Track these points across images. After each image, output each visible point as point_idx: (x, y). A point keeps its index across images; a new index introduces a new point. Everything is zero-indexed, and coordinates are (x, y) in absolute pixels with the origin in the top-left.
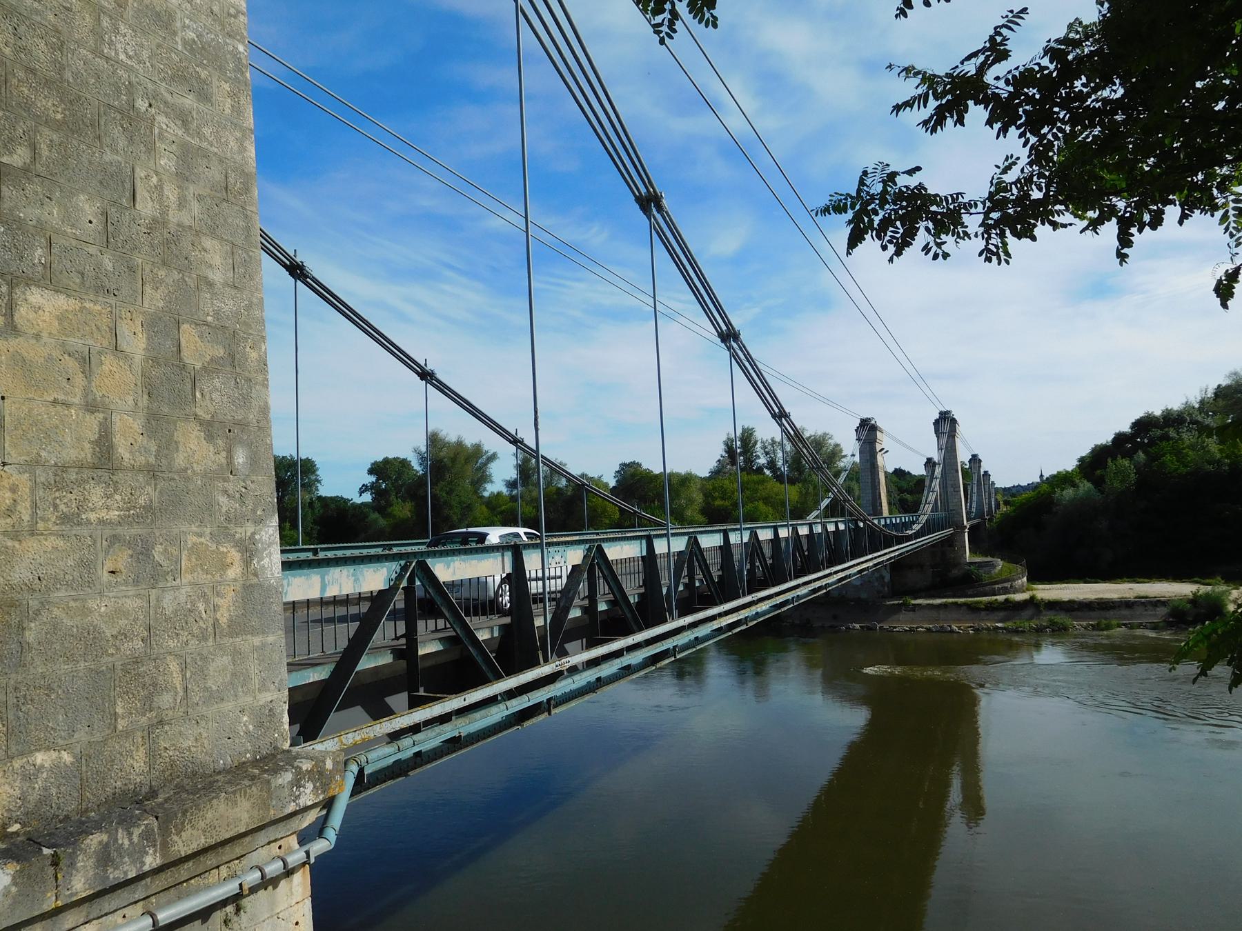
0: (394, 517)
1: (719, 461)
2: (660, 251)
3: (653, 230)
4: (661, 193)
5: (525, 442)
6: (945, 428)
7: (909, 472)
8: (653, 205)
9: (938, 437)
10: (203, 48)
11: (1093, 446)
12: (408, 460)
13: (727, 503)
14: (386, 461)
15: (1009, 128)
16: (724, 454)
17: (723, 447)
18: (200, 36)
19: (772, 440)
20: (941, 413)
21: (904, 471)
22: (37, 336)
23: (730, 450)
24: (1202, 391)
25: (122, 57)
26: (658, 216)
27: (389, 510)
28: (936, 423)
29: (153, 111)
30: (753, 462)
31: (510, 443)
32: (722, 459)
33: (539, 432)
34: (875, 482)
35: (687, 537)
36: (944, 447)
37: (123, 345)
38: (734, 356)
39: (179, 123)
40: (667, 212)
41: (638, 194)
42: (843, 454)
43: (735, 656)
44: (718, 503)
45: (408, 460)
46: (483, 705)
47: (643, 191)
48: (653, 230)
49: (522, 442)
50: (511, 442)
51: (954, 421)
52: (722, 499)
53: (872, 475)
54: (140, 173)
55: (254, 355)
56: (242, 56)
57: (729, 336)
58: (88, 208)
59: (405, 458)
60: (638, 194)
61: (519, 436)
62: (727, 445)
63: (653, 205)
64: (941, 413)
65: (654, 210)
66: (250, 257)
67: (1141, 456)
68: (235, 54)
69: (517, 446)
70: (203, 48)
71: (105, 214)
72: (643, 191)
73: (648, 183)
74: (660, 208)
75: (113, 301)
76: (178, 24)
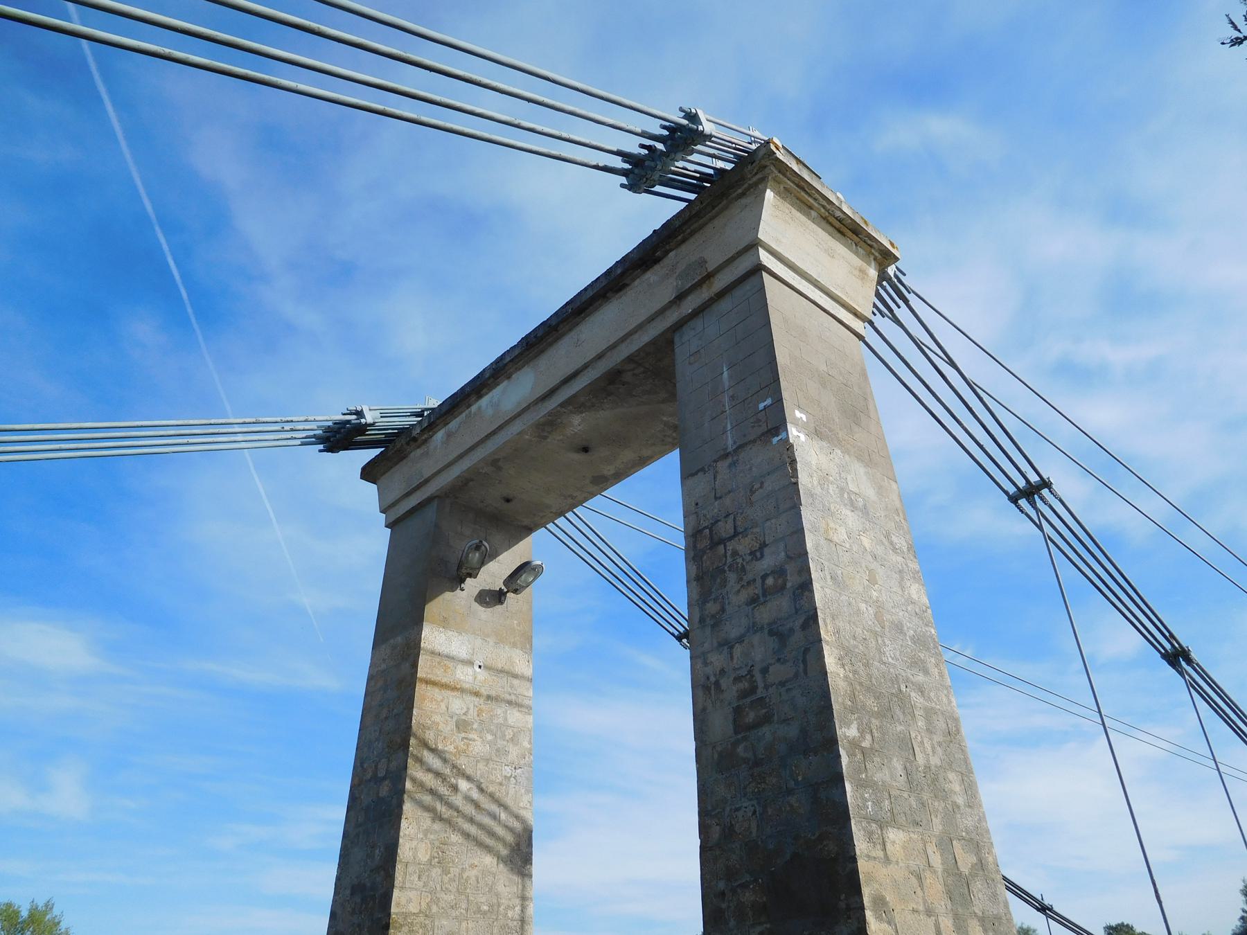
1: (1242, 918)
2: (1202, 705)
3: (1048, 541)
4: (1187, 647)
5: (1055, 909)
8: (1181, 659)
10: (918, 639)
18: (915, 631)
22: (897, 863)
25: (890, 660)
26: (1189, 669)
29: (908, 690)
31: (1038, 911)
33: (1163, 904)
37: (932, 863)
38: (1192, 685)
39: (920, 694)
40: (1197, 664)
41: (1163, 651)
47: (1168, 646)
48: (1038, 523)
49: (1051, 910)
50: (1038, 910)
54: (913, 735)
55: (990, 859)
56: (934, 637)
57: (1177, 657)
58: (898, 765)
60: (1163, 651)
61: (1046, 902)
63: (1181, 659)
65: (1183, 663)
66: (971, 781)
68: (931, 636)
69: (1046, 914)
70: (918, 639)
71: (905, 768)
72: (1168, 646)
73: (1171, 637)
74: (1189, 661)
75: (920, 830)
76: (905, 628)
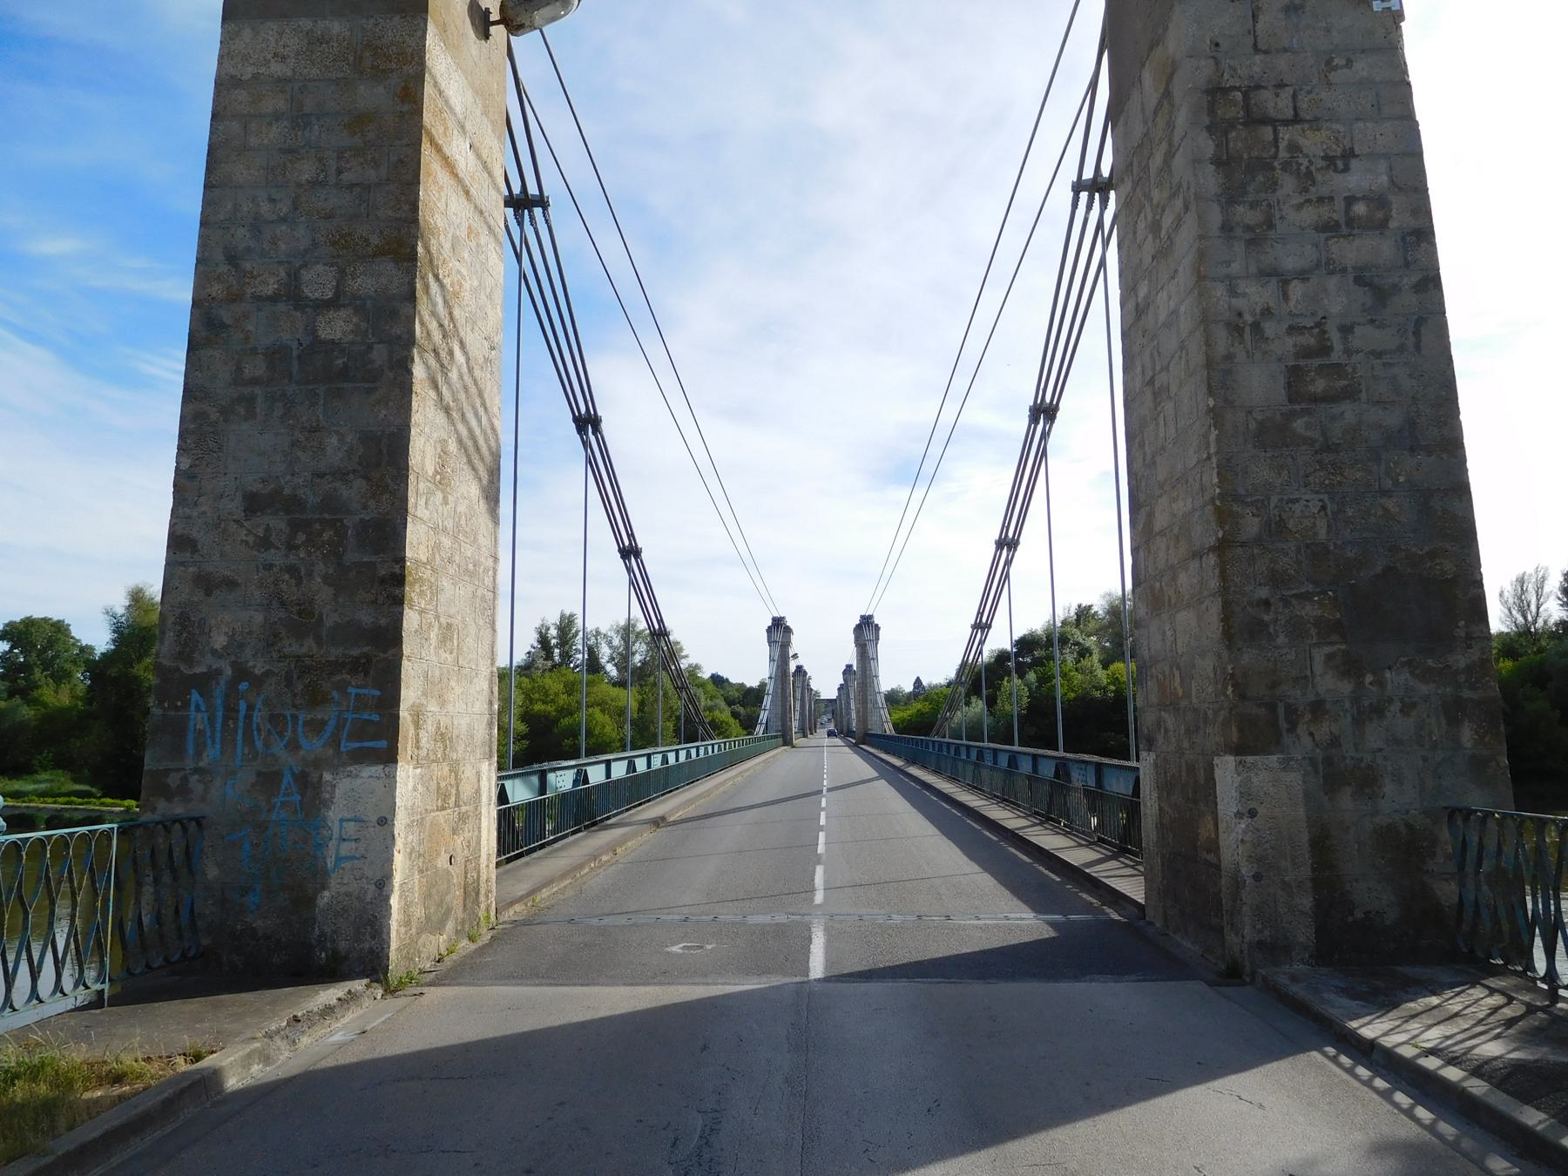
0: (45, 705)
1: (529, 653)
6: (779, 636)
7: (727, 679)
9: (770, 646)
11: (725, 677)
12: (66, 622)
13: (550, 708)
14: (29, 623)
15: (154, 587)
16: (536, 644)
17: (536, 636)
19: (596, 632)
20: (774, 619)
21: (722, 678)
23: (544, 640)
24: (1065, 609)
27: (35, 694)
28: (769, 630)
30: (571, 656)
32: (533, 650)
34: (786, 693)
35: (627, 761)
36: (776, 658)
42: (683, 654)
43: (1454, 1129)
44: (538, 707)
45: (66, 622)
46: (295, 1077)
51: (788, 630)
52: (544, 702)
53: (782, 684)
59: (61, 619)
62: (541, 633)
64: (774, 619)
67: (1031, 676)
